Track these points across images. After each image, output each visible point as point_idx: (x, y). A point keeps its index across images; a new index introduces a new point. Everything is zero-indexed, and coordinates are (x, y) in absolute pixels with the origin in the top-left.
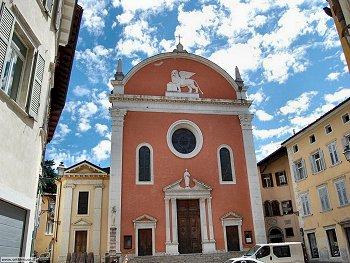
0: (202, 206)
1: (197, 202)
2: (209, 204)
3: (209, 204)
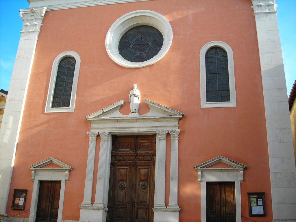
0: (160, 146)
1: (152, 137)
2: (174, 144)
3: (174, 144)
